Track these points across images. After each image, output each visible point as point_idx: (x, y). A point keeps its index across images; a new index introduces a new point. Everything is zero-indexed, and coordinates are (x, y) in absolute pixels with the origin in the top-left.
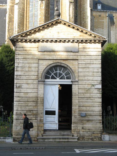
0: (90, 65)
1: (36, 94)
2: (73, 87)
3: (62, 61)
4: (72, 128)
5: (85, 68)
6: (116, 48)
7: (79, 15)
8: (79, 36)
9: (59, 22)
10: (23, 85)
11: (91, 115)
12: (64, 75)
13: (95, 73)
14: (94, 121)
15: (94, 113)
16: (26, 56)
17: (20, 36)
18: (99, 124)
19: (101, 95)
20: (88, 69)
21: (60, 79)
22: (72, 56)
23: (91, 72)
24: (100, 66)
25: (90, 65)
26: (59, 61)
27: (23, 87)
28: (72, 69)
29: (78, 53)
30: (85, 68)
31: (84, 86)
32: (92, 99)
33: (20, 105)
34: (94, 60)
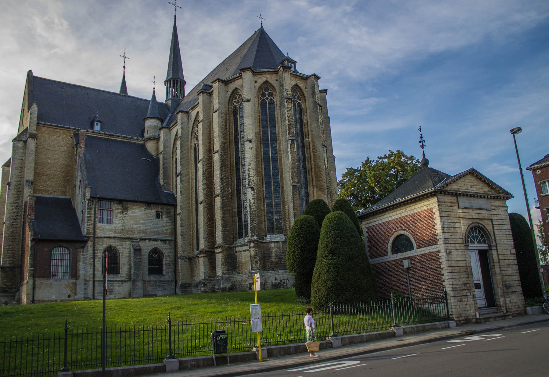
1: (465, 262)
7: (309, 172)
10: (452, 251)
13: (508, 236)
16: (450, 213)
19: (519, 277)
24: (509, 227)
26: (477, 221)
27: (453, 253)
33: (454, 277)
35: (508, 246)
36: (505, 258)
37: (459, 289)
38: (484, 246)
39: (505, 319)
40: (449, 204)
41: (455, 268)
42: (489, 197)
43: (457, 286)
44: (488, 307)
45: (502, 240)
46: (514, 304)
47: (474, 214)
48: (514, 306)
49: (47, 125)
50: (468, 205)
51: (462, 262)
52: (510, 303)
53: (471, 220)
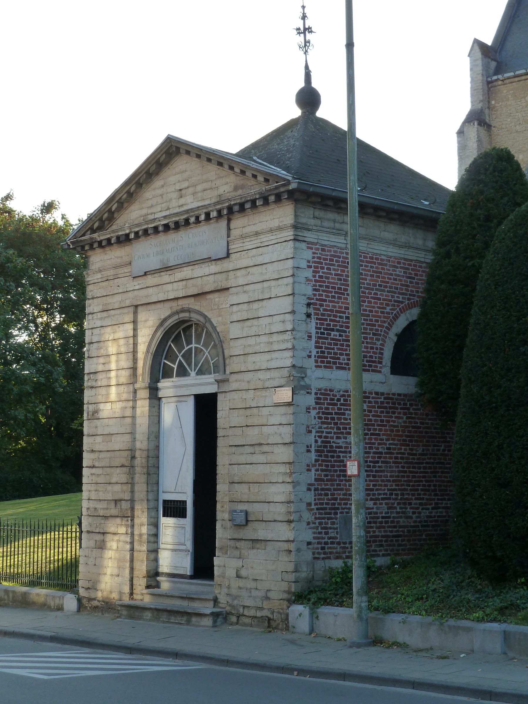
0: (260, 304)
2: (220, 397)
3: (192, 300)
4: (216, 573)
5: (248, 319)
6: (67, 221)
8: (232, 189)
9: (174, 149)
11: (263, 521)
12: (180, 353)
13: (275, 338)
14: (270, 546)
15: (271, 509)
17: (89, 232)
18: (286, 559)
20: (255, 322)
21: (197, 374)
22: (211, 278)
23: (265, 334)
25: (262, 307)
26: (183, 303)
28: (218, 329)
29: (227, 260)
30: (248, 319)
31: (244, 395)
32: (266, 448)
34: (273, 283)
35: (268, 375)
36: (250, 422)
37: (101, 513)
38: (206, 385)
39: (188, 622)
40: (111, 272)
41: (102, 455)
42: (214, 214)
43: (99, 506)
44: (191, 577)
45: (251, 358)
46: (253, 585)
47: (172, 287)
48: (250, 590)
49: (509, 78)
50: (154, 263)
51: (119, 438)
52: (238, 576)
53: (168, 305)
